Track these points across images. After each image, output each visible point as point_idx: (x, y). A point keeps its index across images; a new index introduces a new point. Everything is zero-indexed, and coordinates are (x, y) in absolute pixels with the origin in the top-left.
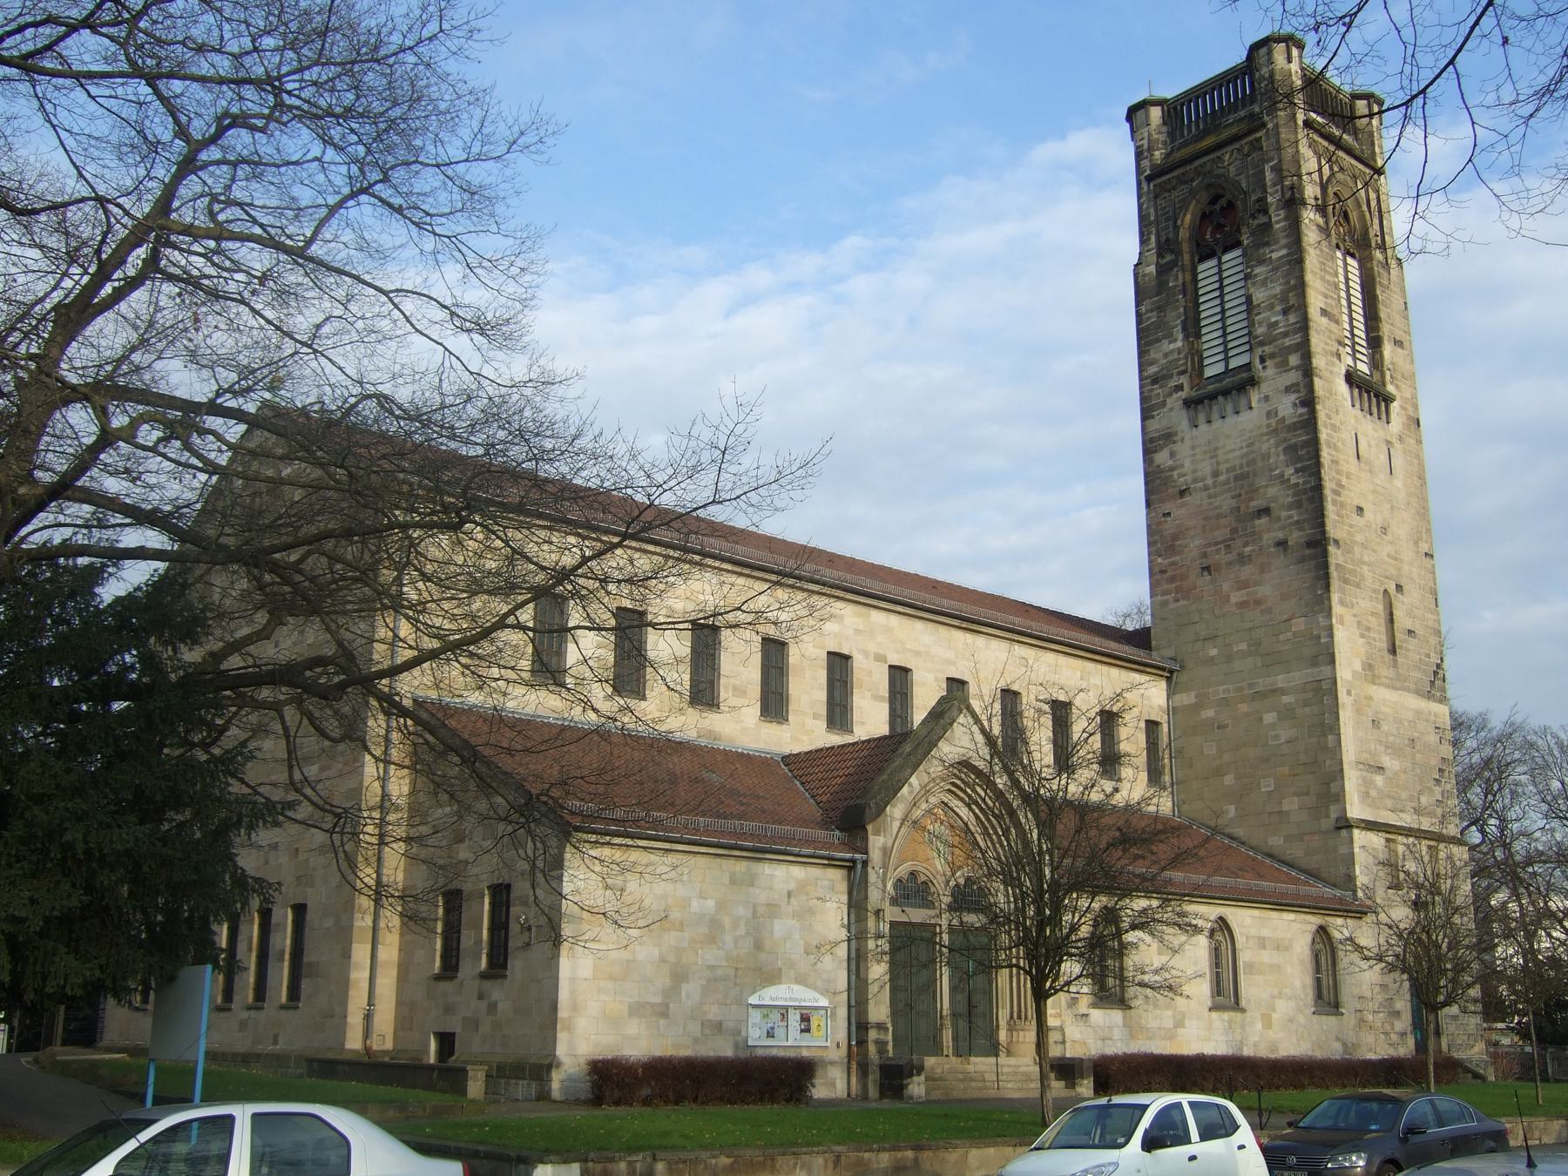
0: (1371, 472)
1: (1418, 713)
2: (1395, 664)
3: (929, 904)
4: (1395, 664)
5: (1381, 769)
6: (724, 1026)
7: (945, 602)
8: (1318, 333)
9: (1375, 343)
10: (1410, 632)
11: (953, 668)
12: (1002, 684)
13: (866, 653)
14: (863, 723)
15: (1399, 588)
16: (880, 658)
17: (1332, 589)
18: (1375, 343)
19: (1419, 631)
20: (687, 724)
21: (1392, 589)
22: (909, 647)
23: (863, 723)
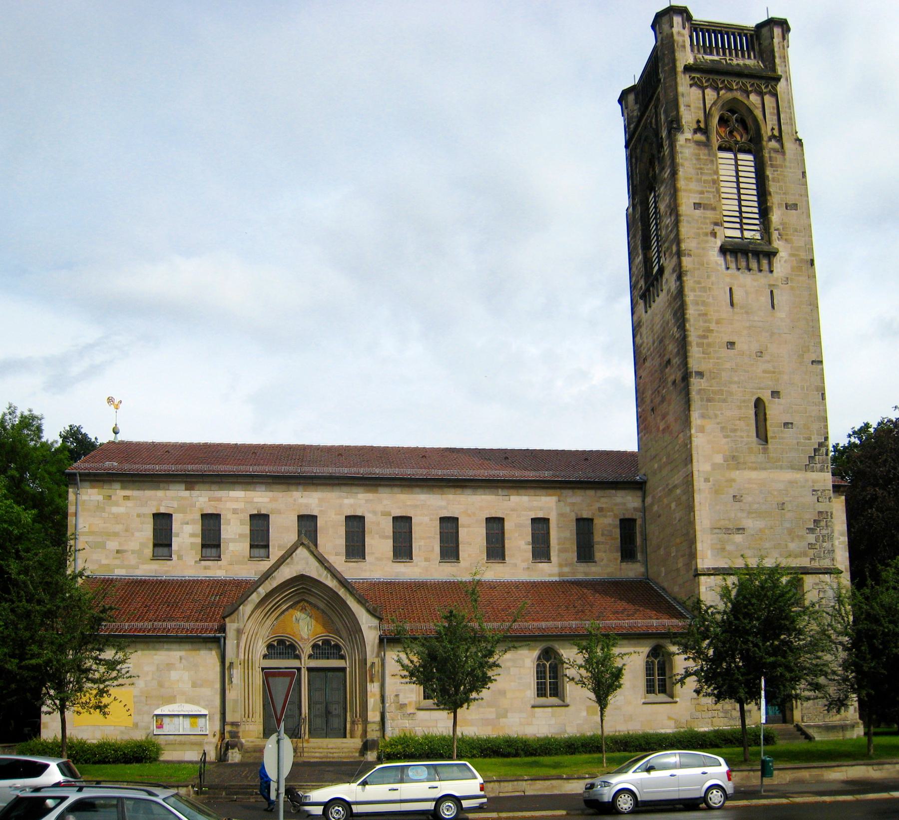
0: (747, 313)
1: (791, 483)
2: (765, 450)
3: (298, 657)
4: (765, 450)
5: (741, 530)
6: (841, 730)
7: (190, 467)
8: (688, 222)
9: (764, 212)
10: (786, 425)
11: (445, 511)
12: (223, 513)
13: (375, 513)
14: (373, 553)
15: (775, 394)
16: (385, 514)
17: (692, 408)
18: (764, 212)
19: (797, 420)
20: (494, 573)
21: (766, 396)
22: (409, 503)
23: (373, 553)
